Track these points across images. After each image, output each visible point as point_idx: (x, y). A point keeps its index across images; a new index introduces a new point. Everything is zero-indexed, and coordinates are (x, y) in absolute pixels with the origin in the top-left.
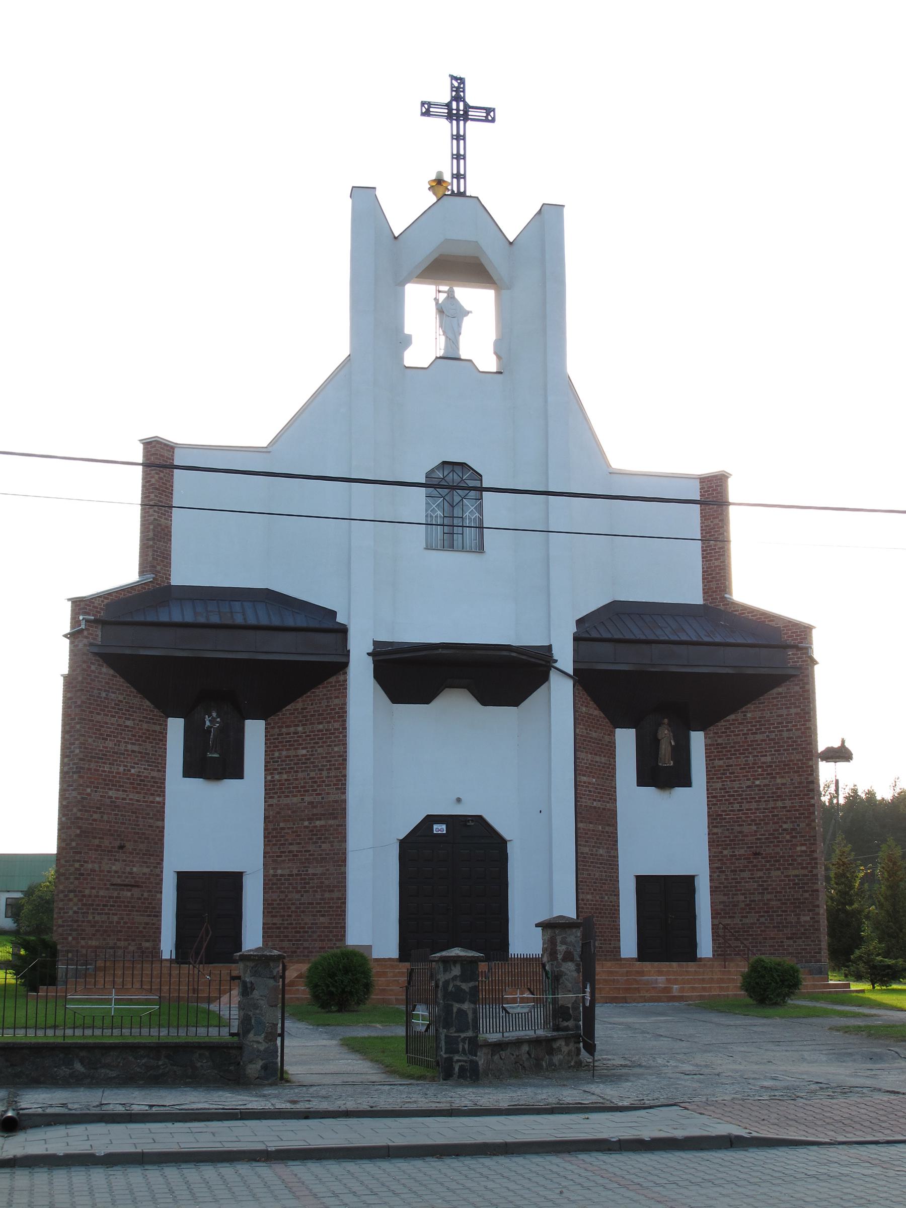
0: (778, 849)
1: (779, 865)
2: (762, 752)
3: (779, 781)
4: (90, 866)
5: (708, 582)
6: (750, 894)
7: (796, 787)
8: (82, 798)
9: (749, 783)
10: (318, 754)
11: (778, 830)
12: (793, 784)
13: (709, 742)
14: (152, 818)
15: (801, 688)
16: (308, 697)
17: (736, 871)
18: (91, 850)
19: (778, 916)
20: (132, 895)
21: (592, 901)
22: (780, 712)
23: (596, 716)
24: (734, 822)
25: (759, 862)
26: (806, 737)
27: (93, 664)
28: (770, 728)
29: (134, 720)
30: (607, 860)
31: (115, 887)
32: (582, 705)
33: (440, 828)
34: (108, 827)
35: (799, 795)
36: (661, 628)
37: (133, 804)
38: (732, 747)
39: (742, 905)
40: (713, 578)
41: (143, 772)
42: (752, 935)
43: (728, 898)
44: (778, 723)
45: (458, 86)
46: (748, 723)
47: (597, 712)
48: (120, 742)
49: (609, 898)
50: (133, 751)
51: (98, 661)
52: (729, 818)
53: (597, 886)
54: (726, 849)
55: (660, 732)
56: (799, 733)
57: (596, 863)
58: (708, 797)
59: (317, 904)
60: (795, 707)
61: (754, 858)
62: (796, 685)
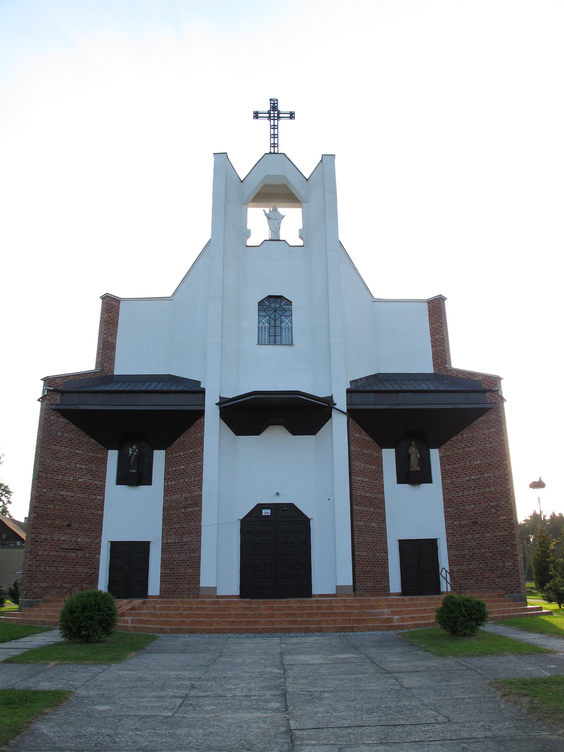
0: (488, 519)
1: (490, 529)
2: (474, 458)
3: (486, 475)
4: (43, 537)
5: (436, 360)
6: (472, 549)
7: (497, 479)
8: (39, 495)
9: (467, 478)
10: (190, 467)
11: (487, 507)
12: (495, 476)
13: (442, 455)
14: (94, 509)
15: (495, 416)
16: (186, 434)
17: (462, 535)
18: (44, 526)
19: (491, 562)
20: (77, 555)
21: (367, 556)
22: (484, 432)
23: (367, 440)
24: (460, 503)
25: (477, 528)
26: (501, 446)
27: (53, 416)
28: (478, 443)
29: (82, 450)
30: (378, 530)
31: (63, 550)
32: (356, 433)
33: (266, 512)
34: (59, 513)
35: (500, 483)
36: (406, 385)
37: (79, 500)
38: (456, 457)
39: (467, 557)
40: (438, 357)
41: (88, 481)
42: (475, 576)
43: (459, 552)
44: (483, 439)
45: (274, 105)
46: (465, 441)
47: (367, 438)
48: (71, 462)
49: (379, 555)
50: (81, 468)
51: (57, 414)
52: (457, 501)
53: (371, 547)
54: (456, 521)
55: (410, 450)
56: (496, 444)
57: (369, 532)
58: (443, 489)
59: (187, 560)
60: (494, 428)
61: (473, 526)
62: (493, 414)
